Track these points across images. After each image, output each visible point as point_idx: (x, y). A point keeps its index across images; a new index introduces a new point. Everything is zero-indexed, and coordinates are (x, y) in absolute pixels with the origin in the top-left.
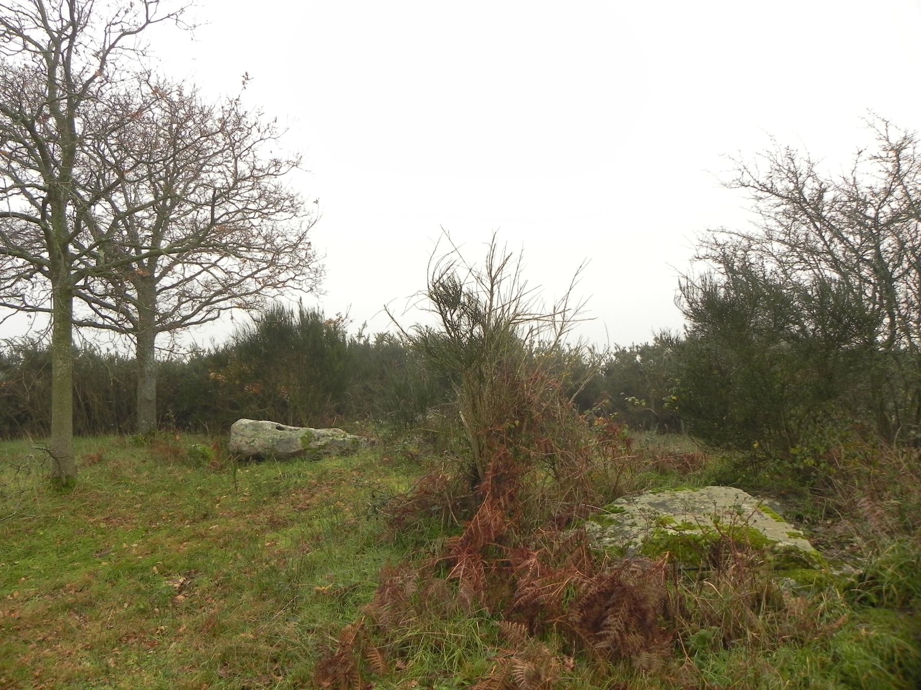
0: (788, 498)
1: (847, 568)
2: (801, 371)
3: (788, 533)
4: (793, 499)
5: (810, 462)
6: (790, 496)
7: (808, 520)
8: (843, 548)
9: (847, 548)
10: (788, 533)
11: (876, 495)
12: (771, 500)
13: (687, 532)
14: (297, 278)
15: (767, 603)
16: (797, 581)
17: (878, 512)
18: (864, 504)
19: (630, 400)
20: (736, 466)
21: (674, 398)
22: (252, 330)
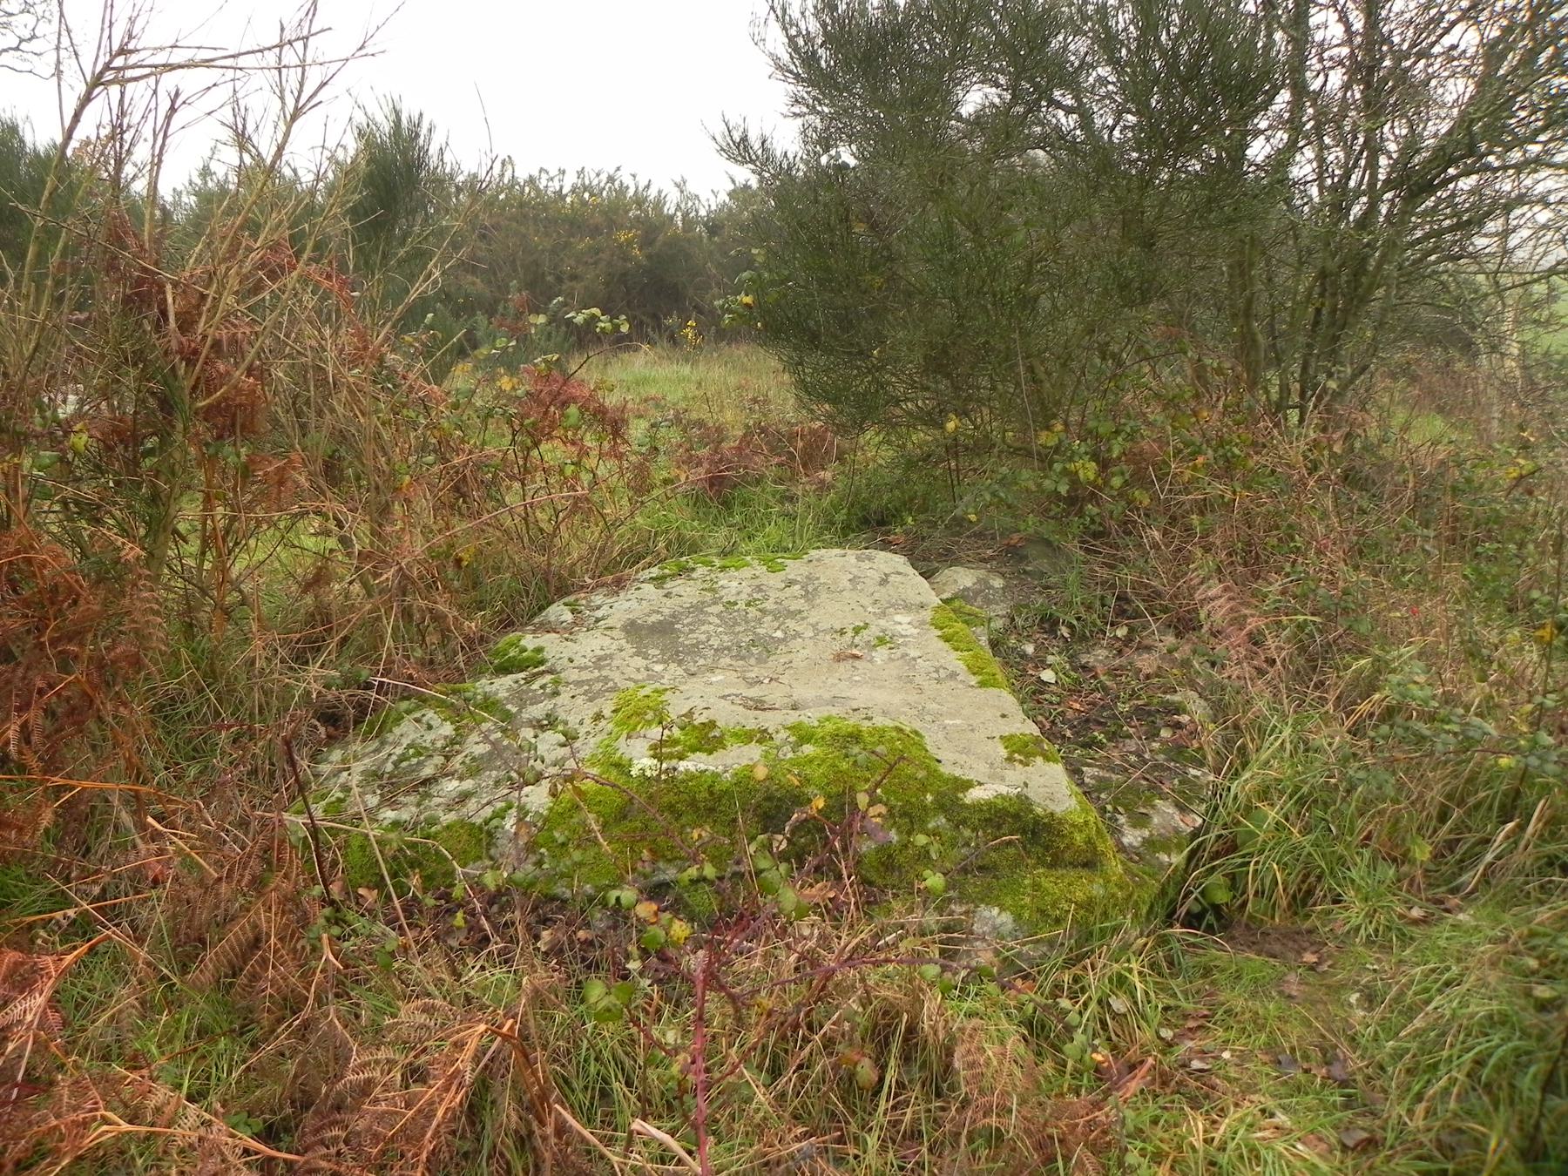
0: (1023, 558)
1: (1165, 815)
2: (1076, 226)
3: (1007, 740)
4: (1038, 562)
5: (1088, 470)
6: (1032, 551)
7: (1071, 626)
8: (1153, 735)
9: (1165, 733)
10: (1007, 740)
11: (1250, 563)
12: (981, 573)
13: (692, 764)
14: (24, 46)
15: (906, 1059)
16: (1018, 918)
17: (1252, 623)
18: (1215, 601)
19: (580, 319)
20: (910, 464)
21: (748, 300)
22: (165, 192)
